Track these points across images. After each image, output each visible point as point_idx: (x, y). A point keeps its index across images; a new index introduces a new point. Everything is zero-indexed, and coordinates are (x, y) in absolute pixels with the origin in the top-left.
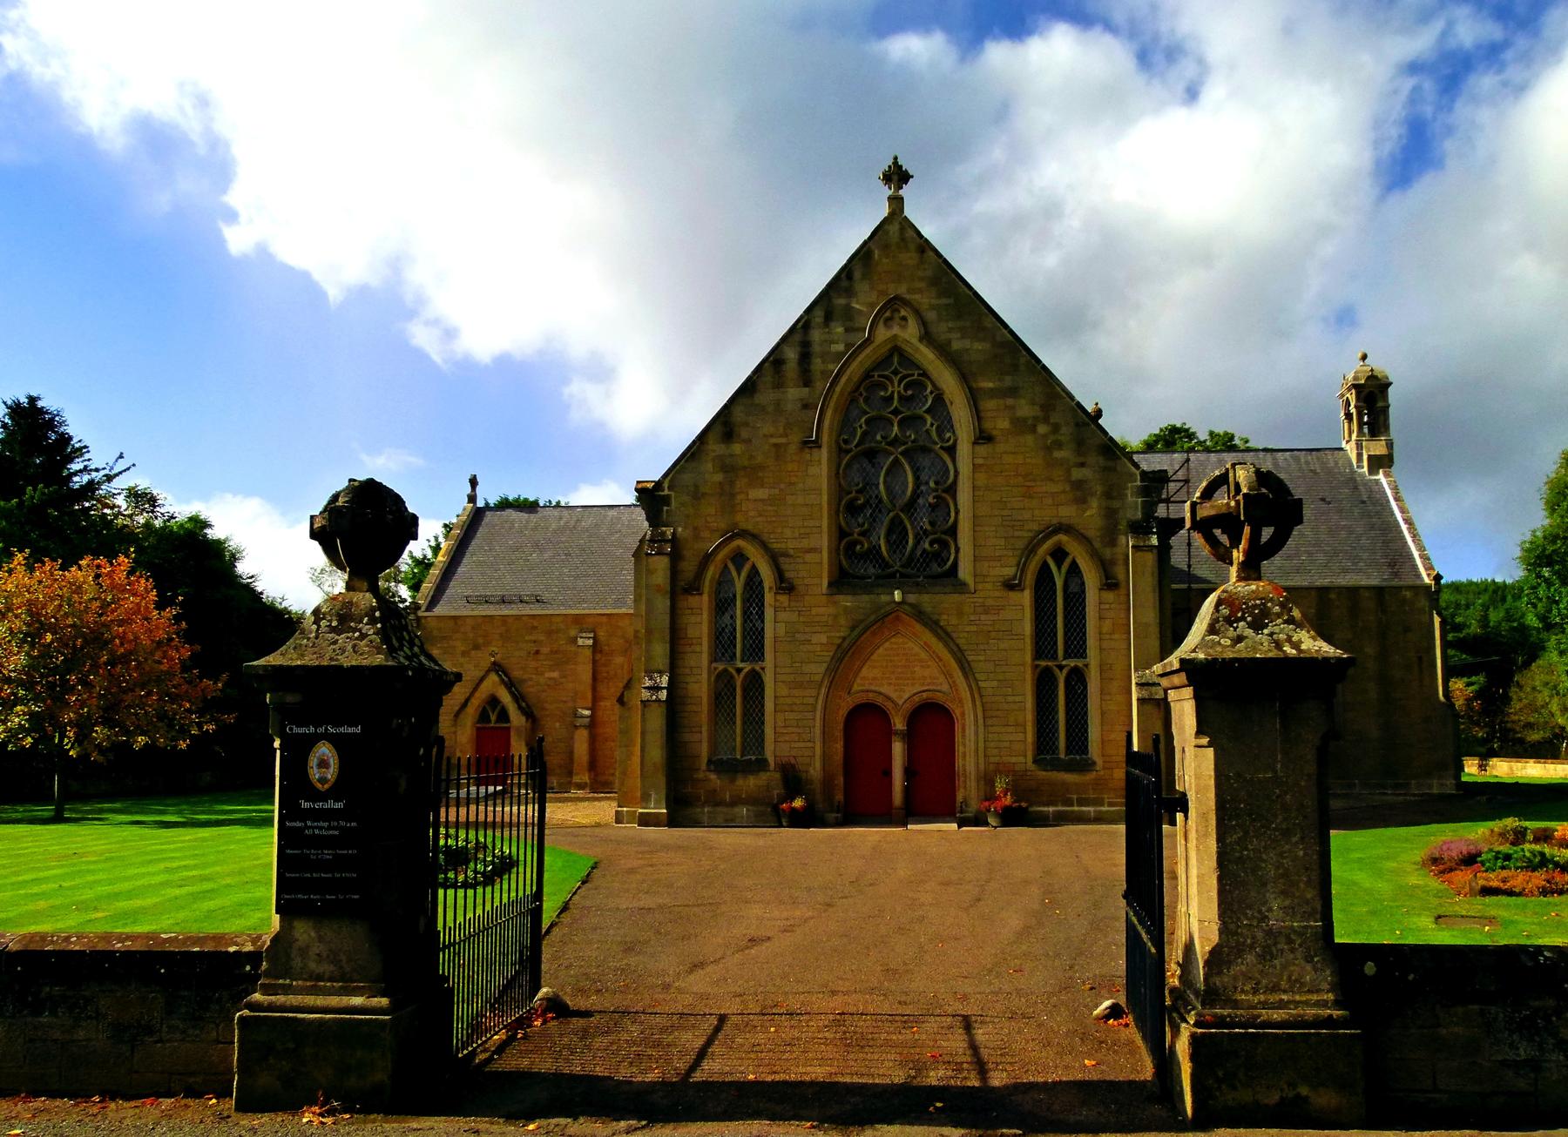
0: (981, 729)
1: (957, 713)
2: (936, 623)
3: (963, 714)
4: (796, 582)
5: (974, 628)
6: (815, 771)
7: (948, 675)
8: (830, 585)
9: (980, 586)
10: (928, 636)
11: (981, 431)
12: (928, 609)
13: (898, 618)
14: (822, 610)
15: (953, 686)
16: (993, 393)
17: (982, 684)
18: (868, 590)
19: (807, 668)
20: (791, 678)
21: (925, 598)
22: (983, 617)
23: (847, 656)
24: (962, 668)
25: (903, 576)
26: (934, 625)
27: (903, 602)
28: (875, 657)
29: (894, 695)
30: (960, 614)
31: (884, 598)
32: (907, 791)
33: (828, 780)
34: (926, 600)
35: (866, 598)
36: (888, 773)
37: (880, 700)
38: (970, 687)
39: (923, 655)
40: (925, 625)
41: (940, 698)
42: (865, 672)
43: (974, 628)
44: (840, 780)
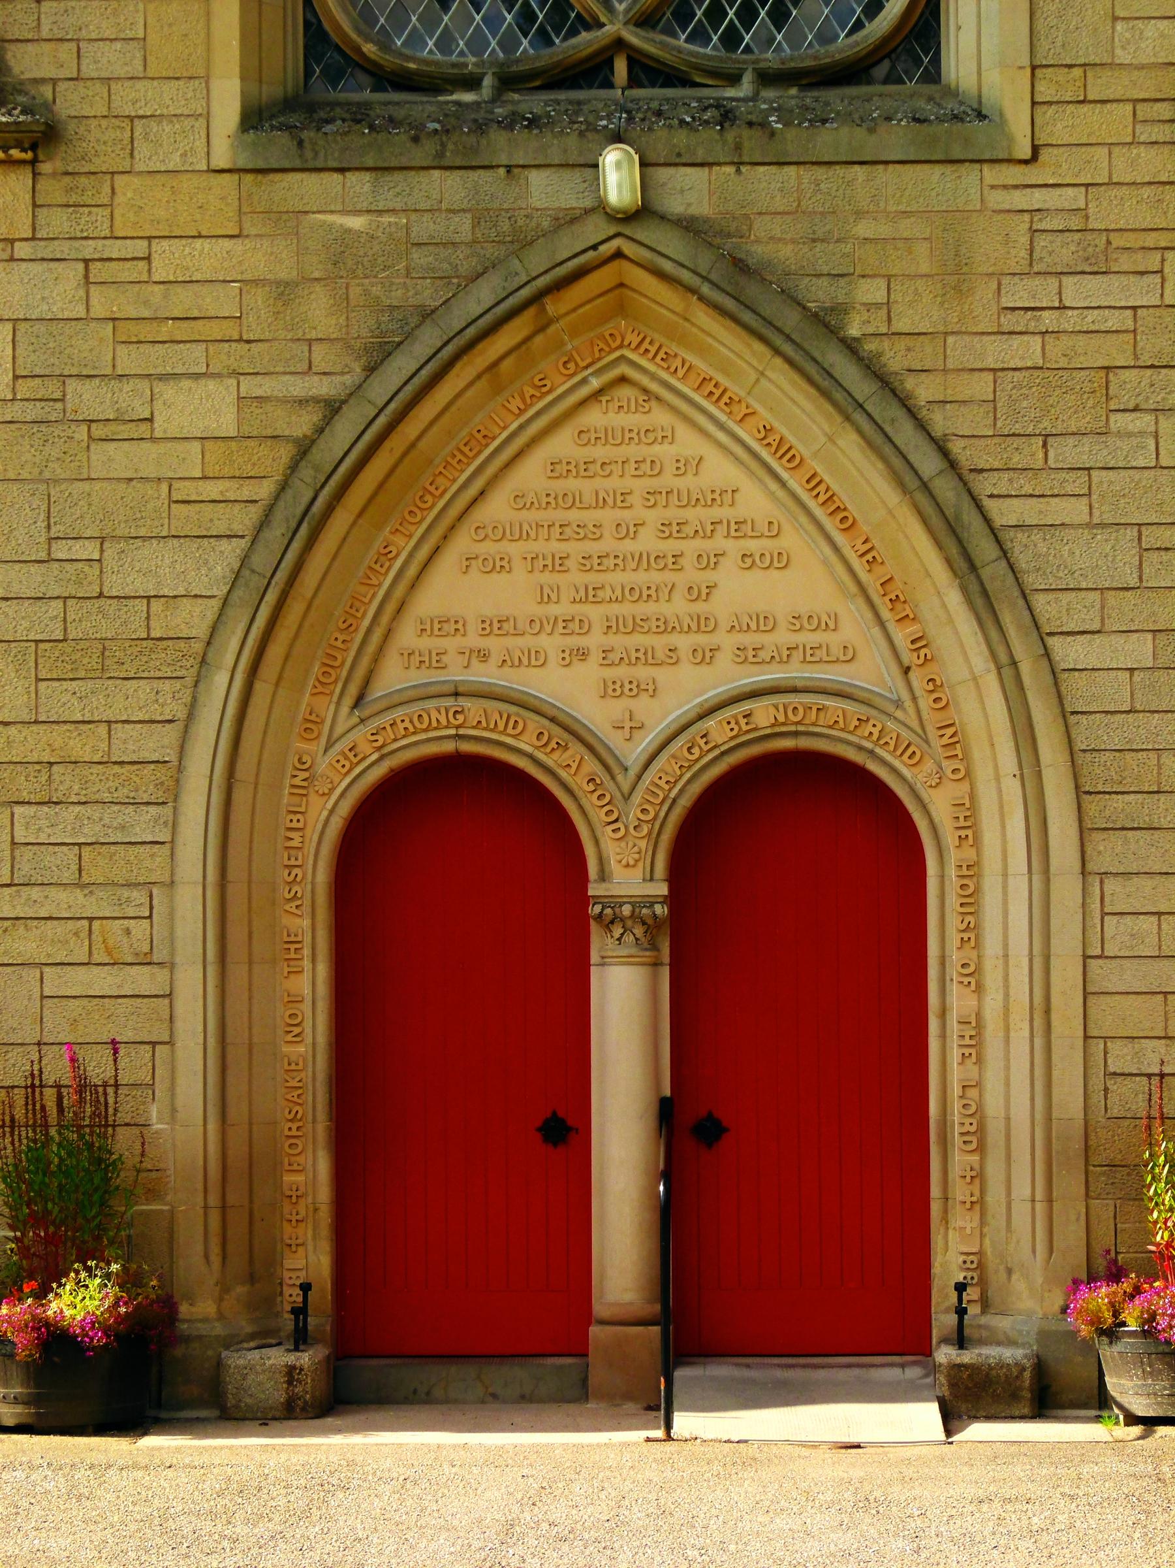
0: (1067, 890)
1: (934, 807)
2: (827, 323)
3: (969, 818)
4: (69, 103)
5: (1030, 350)
6: (174, 1117)
7: (886, 602)
8: (253, 118)
9: (1060, 126)
10: (783, 399)
11: (316, 36)
12: (774, 242)
13: (620, 301)
14: (207, 258)
15: (916, 659)
16: (326, 160)
17: (1004, 513)
18: (457, 145)
19: (133, 571)
20: (47, 621)
21: (768, 186)
22: (1076, 291)
23: (346, 496)
24: (965, 567)
25: (647, 71)
26: (810, 334)
27: (642, 213)
28: (497, 508)
29: (596, 714)
30: (955, 277)
31: (546, 191)
32: (675, 1220)
33: (243, 1176)
34: (769, 200)
35: (448, 187)
36: (566, 1131)
37: (522, 746)
38: (1007, 668)
39: (755, 501)
40: (762, 331)
41: (839, 733)
42: (450, 590)
43: (1030, 350)
44: (313, 1172)
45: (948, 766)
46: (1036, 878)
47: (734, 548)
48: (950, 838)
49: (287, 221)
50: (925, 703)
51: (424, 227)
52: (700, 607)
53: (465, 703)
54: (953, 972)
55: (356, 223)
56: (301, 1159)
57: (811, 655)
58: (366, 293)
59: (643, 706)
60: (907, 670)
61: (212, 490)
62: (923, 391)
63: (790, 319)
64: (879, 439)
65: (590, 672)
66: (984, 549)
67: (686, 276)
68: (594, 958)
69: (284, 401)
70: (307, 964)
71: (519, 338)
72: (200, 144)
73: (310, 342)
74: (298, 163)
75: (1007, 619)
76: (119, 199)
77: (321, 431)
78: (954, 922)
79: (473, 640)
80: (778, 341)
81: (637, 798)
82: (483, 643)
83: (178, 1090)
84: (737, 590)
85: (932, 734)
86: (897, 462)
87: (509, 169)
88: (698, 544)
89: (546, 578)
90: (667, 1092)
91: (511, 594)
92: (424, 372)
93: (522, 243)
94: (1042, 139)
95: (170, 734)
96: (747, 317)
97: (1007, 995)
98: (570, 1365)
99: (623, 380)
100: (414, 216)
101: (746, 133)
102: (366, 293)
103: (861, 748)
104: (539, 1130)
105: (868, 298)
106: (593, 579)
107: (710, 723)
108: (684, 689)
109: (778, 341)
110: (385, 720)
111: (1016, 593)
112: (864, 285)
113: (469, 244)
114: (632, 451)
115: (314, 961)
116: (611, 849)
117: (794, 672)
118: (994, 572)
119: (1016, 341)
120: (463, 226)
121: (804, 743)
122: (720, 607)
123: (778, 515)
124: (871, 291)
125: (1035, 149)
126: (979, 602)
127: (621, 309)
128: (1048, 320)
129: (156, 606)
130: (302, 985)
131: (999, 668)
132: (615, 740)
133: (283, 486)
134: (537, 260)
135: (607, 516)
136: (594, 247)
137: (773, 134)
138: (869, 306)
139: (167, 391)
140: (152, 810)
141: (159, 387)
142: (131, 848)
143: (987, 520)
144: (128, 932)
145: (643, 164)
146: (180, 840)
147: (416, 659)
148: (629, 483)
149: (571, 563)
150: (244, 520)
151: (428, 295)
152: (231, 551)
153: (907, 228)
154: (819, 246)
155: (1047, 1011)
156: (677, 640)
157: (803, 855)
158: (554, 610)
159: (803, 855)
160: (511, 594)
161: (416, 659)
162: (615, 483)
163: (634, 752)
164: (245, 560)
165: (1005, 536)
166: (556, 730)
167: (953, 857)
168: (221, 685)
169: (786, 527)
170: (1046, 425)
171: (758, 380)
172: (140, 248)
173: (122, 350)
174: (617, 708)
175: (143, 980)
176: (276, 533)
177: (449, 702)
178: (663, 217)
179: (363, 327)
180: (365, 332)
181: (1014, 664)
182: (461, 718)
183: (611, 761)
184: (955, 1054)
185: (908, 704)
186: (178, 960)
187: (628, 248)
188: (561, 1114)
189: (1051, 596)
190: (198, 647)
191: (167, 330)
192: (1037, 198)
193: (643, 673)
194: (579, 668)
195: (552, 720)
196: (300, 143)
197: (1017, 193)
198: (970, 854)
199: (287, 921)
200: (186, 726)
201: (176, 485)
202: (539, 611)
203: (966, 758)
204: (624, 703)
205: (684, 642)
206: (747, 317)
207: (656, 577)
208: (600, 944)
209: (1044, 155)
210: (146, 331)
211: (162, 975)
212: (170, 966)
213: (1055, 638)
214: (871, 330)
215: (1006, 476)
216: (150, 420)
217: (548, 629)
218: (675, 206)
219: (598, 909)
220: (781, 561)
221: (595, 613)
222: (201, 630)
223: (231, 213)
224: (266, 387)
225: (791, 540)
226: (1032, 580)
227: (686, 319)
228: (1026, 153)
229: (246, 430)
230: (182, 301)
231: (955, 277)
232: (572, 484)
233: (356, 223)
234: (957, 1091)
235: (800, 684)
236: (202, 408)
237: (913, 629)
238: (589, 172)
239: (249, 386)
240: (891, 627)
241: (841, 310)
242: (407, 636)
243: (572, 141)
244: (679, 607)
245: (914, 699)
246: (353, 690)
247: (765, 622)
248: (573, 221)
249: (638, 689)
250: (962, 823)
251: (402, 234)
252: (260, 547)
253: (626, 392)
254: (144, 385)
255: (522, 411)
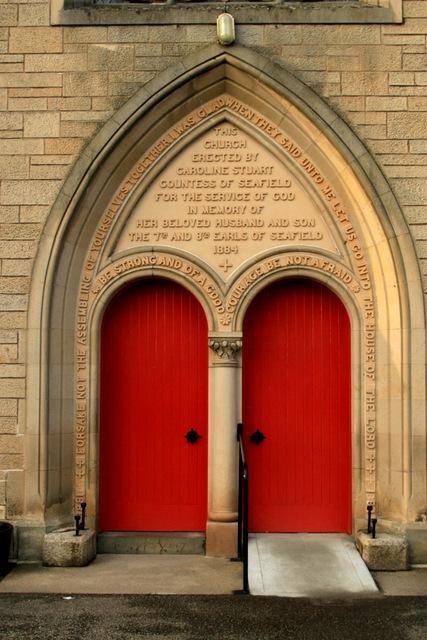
1: (355, 301)
2: (315, 90)
7: (337, 213)
12: (293, 58)
14: (49, 62)
15: (351, 237)
17: (391, 173)
21: (288, 33)
26: (310, 96)
29: (212, 261)
31: (192, 34)
35: (154, 33)
36: (197, 437)
37: (181, 274)
41: (314, 268)
42: (149, 209)
45: (363, 283)
46: (405, 331)
47: (271, 192)
48: (364, 314)
49: (82, 47)
50: (353, 256)
51: (143, 50)
52: (257, 217)
53: (155, 254)
54: (364, 372)
55: (112, 48)
56: (84, 449)
57: (304, 237)
58: (116, 77)
59: (232, 257)
60: (345, 243)
61: (48, 160)
62: (356, 120)
63: (299, 89)
64: (337, 141)
65: (210, 243)
66: (382, 187)
67: (253, 70)
68: (210, 364)
69: (80, 122)
70: (87, 365)
71: (182, 98)
72: (47, 15)
73: (92, 98)
74: (88, 23)
75: (392, 218)
76: (11, 38)
77: (95, 135)
78: (365, 350)
79: (160, 230)
80: (293, 98)
81: (230, 296)
82: (163, 231)
83: (28, 419)
84: (272, 210)
85: (356, 269)
86: (345, 150)
87: (178, 25)
88: (256, 190)
89: (193, 204)
90: (241, 422)
91: (178, 210)
92: (140, 110)
93: (181, 56)
94: (407, 15)
95: (28, 264)
96: (279, 87)
97: (389, 381)
98: (198, 538)
99: (225, 121)
100: (137, 45)
101: (280, 11)
102: (116, 77)
103: (326, 275)
104: (264, 438)
105: (332, 81)
106: (212, 204)
107: (261, 264)
108: (249, 252)
109: (293, 98)
110: (122, 261)
111: (396, 206)
112: (331, 75)
113: (162, 56)
114: (229, 151)
115: (90, 364)
116: (218, 318)
117: (296, 244)
118: (387, 197)
119: (396, 99)
120: (158, 49)
121: (301, 273)
122: (266, 216)
123: (289, 177)
124: (333, 78)
125: (404, 19)
126: (380, 210)
127: (224, 90)
128: (410, 91)
129: (23, 209)
130: (84, 374)
131: (388, 240)
132: (220, 272)
133: (79, 158)
134: (190, 64)
135: (218, 178)
136: (214, 58)
137: (291, 11)
138: (332, 84)
139: (30, 118)
140: (19, 297)
141: (26, 116)
142: (10, 314)
143: (384, 176)
144: (8, 350)
145: (236, 24)
146: (31, 310)
147: (135, 238)
148: (227, 164)
149: (202, 198)
150: (61, 172)
151: (143, 78)
152: (55, 187)
153: (348, 52)
154: (311, 59)
155: (410, 388)
156: (246, 230)
157: (298, 311)
158: (194, 217)
159: (298, 311)
160: (178, 210)
161: (135, 238)
162: (222, 165)
163: (228, 278)
164: (61, 190)
165: (392, 182)
166: (195, 267)
167: (365, 322)
168: (50, 245)
169: (293, 183)
170: (409, 135)
171: (283, 119)
172: (20, 58)
173: (11, 100)
174: (221, 259)
175: (14, 371)
176: (75, 178)
177: (150, 254)
178: (244, 46)
179: (114, 91)
180: (115, 93)
181: (395, 237)
182: (154, 261)
183: (218, 280)
184: (365, 407)
185: (346, 257)
186: (29, 362)
187: (229, 59)
188: (186, 434)
189: (411, 208)
190: (40, 227)
191: (31, 92)
192: (404, 40)
193: (232, 244)
194: (205, 241)
195: (194, 262)
196: (89, 14)
197: (396, 38)
198: (372, 321)
199: (79, 347)
200: (35, 262)
201: (33, 157)
202: (188, 218)
203: (371, 280)
204: (224, 256)
205: (250, 231)
206: (279, 87)
207: (237, 204)
208: (213, 358)
209: (408, 22)
210: (21, 93)
211: (22, 369)
212: (25, 364)
213: (414, 227)
214: (333, 94)
215: (392, 157)
216: (22, 130)
217: (192, 224)
218: (249, 41)
219: (212, 343)
220: (291, 198)
221: (212, 219)
222: (42, 220)
223: (59, 42)
224: (72, 116)
225: (295, 189)
226: (403, 202)
227: (253, 92)
228: (400, 20)
229: (63, 135)
230: (38, 80)
231: (370, 72)
232: (203, 165)
233: (112, 48)
234: (366, 422)
235: (299, 248)
236: (47, 125)
237: (348, 225)
238: (212, 27)
239: (66, 116)
240: (339, 225)
241: (320, 85)
242: (132, 228)
243: (205, 14)
244: (248, 217)
245: (348, 255)
246: (108, 249)
247: (284, 224)
248: (207, 47)
249: (230, 251)
250: (369, 307)
251: (131, 53)
252: (68, 184)
253: (226, 127)
254: (20, 115)
255: (182, 133)
